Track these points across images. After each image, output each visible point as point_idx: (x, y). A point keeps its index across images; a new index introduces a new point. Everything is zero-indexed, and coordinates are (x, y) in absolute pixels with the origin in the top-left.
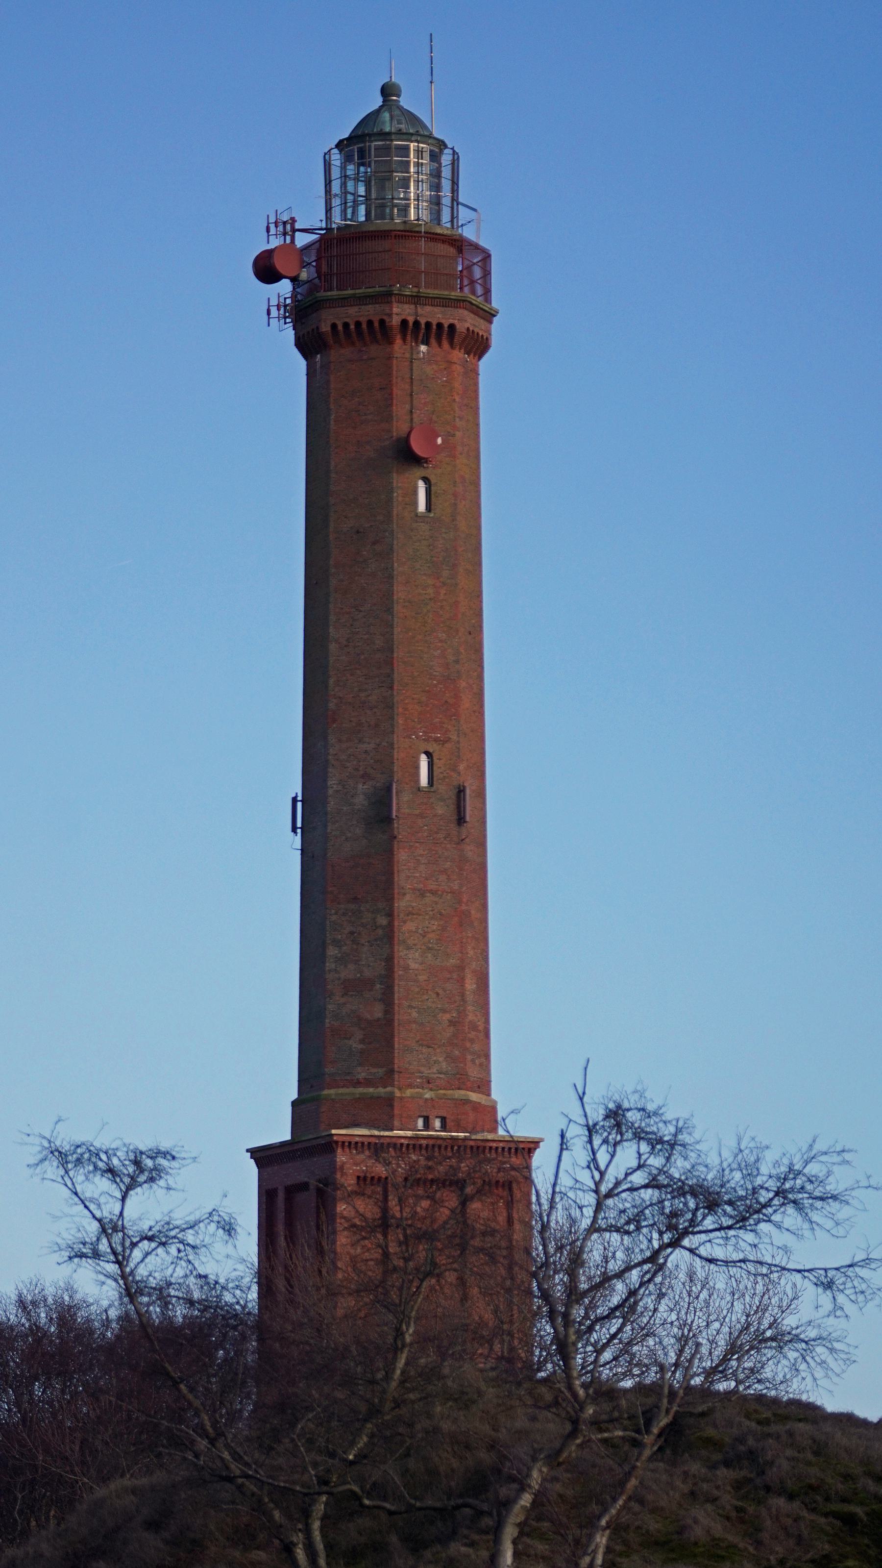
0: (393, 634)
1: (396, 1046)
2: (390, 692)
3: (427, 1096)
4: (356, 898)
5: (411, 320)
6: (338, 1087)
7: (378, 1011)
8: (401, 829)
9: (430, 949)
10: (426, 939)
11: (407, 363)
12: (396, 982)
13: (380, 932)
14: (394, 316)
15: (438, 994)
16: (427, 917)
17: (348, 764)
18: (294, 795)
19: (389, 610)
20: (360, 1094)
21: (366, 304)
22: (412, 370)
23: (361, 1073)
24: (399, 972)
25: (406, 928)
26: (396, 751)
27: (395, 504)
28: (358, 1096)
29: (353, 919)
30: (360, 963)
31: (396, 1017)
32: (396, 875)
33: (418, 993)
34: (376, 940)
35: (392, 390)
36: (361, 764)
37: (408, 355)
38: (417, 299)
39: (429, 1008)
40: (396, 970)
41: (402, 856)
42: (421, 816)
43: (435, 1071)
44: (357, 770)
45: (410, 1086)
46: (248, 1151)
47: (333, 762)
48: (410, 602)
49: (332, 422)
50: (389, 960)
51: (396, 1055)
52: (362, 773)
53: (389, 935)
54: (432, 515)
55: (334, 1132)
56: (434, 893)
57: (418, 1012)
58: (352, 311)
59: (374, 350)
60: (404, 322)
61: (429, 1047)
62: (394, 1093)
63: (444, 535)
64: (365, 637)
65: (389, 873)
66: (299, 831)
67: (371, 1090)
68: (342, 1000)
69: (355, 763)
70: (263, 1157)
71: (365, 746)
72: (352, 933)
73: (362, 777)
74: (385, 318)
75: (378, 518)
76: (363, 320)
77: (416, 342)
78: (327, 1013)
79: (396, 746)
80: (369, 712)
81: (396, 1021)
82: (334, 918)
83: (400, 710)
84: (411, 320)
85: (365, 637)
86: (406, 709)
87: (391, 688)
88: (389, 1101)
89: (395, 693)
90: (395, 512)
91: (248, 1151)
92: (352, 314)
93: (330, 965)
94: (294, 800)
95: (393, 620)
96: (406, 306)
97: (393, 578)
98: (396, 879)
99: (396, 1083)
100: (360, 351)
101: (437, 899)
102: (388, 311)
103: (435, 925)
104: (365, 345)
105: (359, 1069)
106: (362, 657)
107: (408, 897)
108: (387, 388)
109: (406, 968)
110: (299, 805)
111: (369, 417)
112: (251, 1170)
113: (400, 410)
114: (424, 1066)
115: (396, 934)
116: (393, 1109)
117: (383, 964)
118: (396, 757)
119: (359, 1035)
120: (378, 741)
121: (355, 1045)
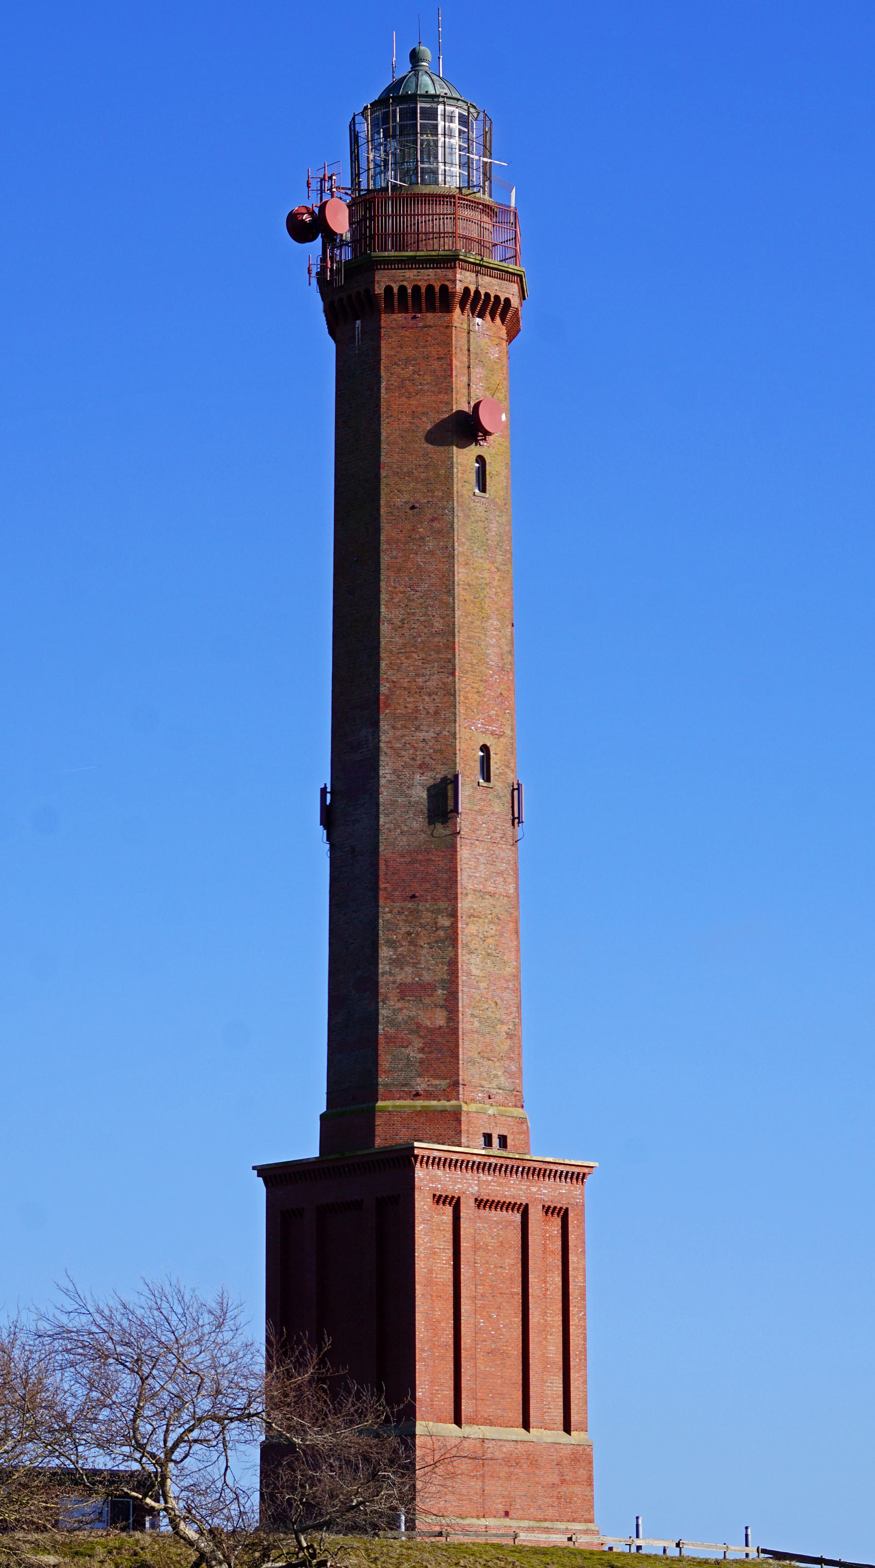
0: (454, 617)
1: (461, 1057)
2: (451, 678)
3: (490, 1112)
4: (413, 896)
5: (472, 288)
6: (394, 1099)
7: (440, 1019)
8: (464, 822)
9: (489, 955)
10: (486, 944)
11: (466, 334)
12: (460, 987)
13: (442, 933)
14: (458, 282)
15: (496, 1003)
16: (486, 921)
17: (403, 753)
18: (323, 786)
19: (450, 592)
20: (422, 1107)
21: (427, 268)
22: (469, 341)
23: (421, 1084)
24: (462, 978)
25: (467, 930)
26: (458, 741)
27: (455, 480)
28: (419, 1109)
30: (419, 966)
31: (460, 1026)
32: (459, 874)
33: (479, 1001)
34: (436, 942)
35: (451, 360)
36: (418, 753)
37: (465, 326)
38: (479, 268)
39: (489, 1018)
40: (460, 974)
41: (464, 853)
42: (480, 812)
43: (494, 1085)
44: (414, 759)
45: (473, 1100)
46: (254, 1168)
47: (385, 750)
48: (469, 585)
49: (383, 391)
50: (453, 965)
51: (461, 1066)
52: (419, 762)
53: (452, 937)
54: (487, 495)
55: (416, 1144)
56: (492, 895)
57: (480, 1022)
58: (411, 274)
59: (430, 317)
60: (467, 290)
61: (489, 1060)
62: (461, 1106)
63: (497, 518)
64: (422, 619)
65: (453, 871)
67: (434, 1103)
68: (399, 1005)
69: (411, 752)
70: (275, 1176)
71: (421, 735)
72: (409, 934)
73: (420, 767)
74: (447, 283)
75: (436, 494)
76: (423, 285)
77: (473, 314)
78: (380, 1018)
79: (458, 736)
80: (427, 698)
81: (460, 1030)
83: (462, 698)
84: (472, 288)
85: (422, 619)
86: (466, 698)
87: (453, 674)
88: (456, 1116)
89: (457, 680)
90: (455, 489)
91: (254, 1168)
92: (410, 277)
93: (383, 967)
94: (323, 791)
95: (454, 603)
96: (468, 274)
97: (453, 557)
98: (459, 878)
99: (461, 1096)
100: (414, 318)
101: (494, 903)
102: (451, 277)
103: (493, 930)
104: (420, 312)
105: (419, 1080)
106: (419, 640)
107: (470, 897)
108: (446, 359)
109: (469, 974)
110: (329, 796)
111: (426, 388)
112: (259, 1187)
113: (459, 381)
114: (485, 1080)
115: (460, 937)
116: (460, 1124)
117: (446, 968)
118: (458, 748)
119: (418, 1043)
120: (438, 729)
121: (413, 1053)
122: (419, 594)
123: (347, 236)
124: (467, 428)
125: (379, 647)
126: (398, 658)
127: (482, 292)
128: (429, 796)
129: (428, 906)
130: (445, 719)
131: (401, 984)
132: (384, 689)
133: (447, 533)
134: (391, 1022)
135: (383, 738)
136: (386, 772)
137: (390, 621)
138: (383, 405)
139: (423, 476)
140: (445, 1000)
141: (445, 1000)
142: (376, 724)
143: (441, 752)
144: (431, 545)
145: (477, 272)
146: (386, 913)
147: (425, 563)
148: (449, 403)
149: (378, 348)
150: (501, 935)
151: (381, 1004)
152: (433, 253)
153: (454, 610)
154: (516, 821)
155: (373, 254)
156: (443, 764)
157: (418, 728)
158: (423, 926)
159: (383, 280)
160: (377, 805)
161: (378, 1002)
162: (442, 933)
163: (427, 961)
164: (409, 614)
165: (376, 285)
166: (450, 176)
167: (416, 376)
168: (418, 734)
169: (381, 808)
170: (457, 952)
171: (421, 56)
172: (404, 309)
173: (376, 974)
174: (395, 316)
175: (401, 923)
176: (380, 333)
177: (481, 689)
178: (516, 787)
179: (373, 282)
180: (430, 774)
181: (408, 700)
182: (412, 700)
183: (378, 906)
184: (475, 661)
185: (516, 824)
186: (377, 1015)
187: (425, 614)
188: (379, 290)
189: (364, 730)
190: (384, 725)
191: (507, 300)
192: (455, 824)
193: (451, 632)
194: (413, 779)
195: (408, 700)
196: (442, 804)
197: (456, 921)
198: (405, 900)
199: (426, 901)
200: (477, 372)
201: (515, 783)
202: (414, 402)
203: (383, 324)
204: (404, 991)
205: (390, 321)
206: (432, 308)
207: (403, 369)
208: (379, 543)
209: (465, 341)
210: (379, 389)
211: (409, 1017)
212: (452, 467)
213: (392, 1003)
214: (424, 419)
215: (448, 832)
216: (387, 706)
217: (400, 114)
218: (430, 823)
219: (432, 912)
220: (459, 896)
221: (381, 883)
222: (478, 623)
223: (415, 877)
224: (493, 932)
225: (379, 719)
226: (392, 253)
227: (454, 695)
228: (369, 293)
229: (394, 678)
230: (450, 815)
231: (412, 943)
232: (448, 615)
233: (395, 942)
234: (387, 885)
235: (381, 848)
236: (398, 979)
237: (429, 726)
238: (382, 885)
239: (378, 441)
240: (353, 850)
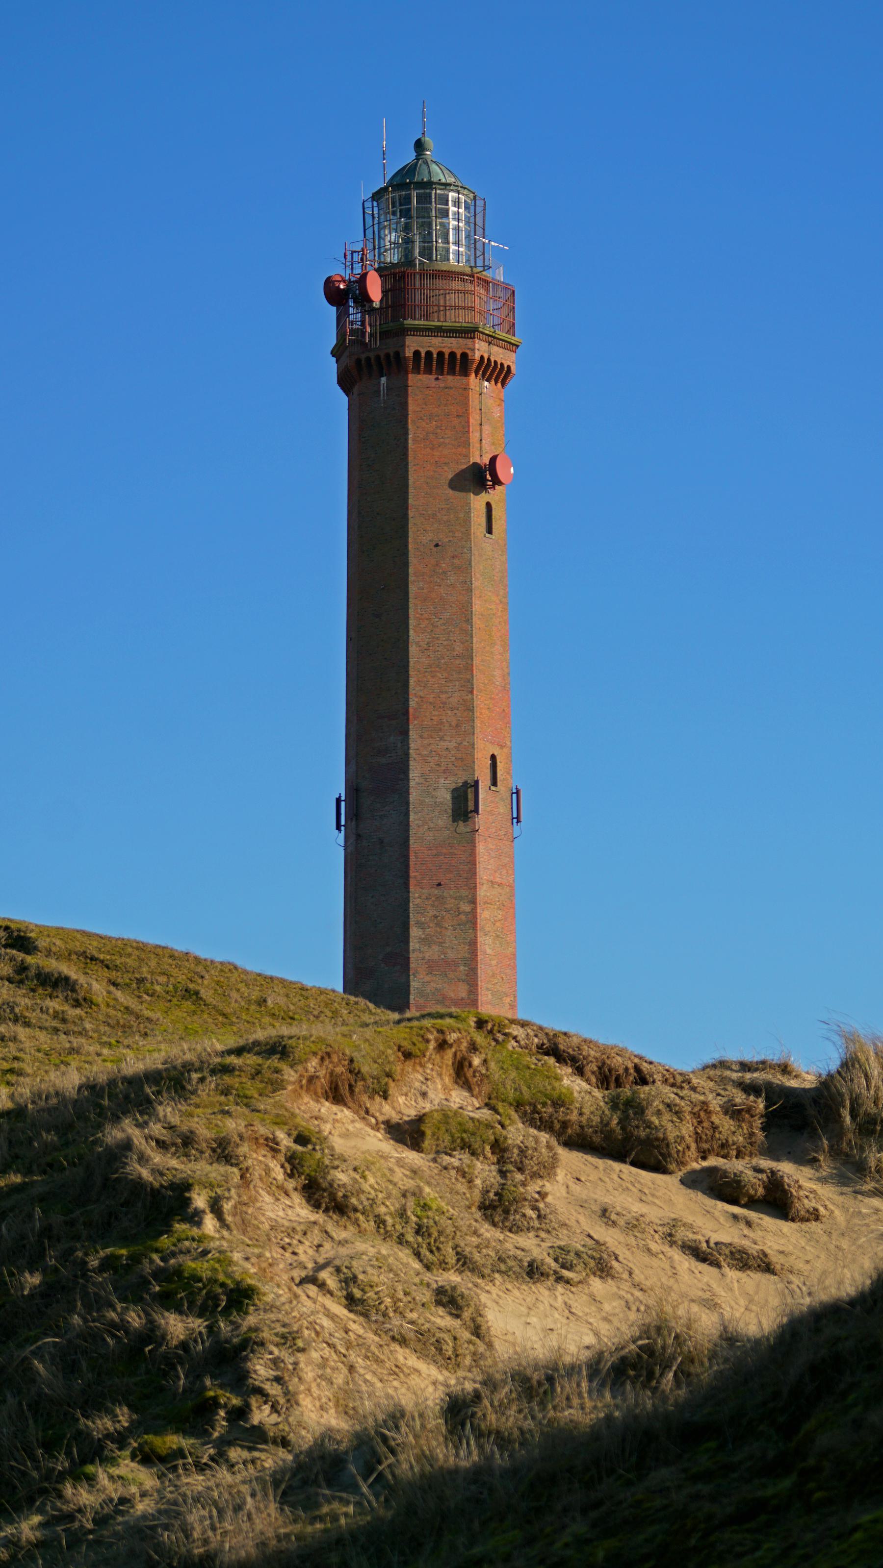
2: (470, 696)
5: (486, 356)
7: (462, 991)
8: (481, 820)
9: (498, 936)
11: (478, 396)
13: (463, 917)
14: (476, 351)
17: (430, 759)
19: (469, 621)
22: (480, 402)
24: (480, 957)
25: (484, 915)
29: (436, 903)
35: (469, 418)
37: (478, 389)
38: (492, 339)
41: (481, 848)
49: (410, 442)
50: (473, 944)
57: (492, 995)
60: (482, 357)
64: (445, 643)
65: (473, 863)
66: (343, 828)
68: (427, 978)
69: (437, 758)
72: (436, 917)
73: (444, 772)
74: (467, 351)
75: (456, 534)
76: (447, 352)
78: (412, 989)
80: (449, 712)
82: (418, 900)
85: (445, 643)
86: (481, 714)
87: (472, 692)
93: (413, 944)
94: (338, 801)
100: (437, 379)
102: (471, 346)
104: (442, 374)
108: (464, 415)
109: (485, 953)
110: (343, 804)
122: (442, 621)
123: (376, 304)
124: (481, 477)
125: (408, 666)
126: (425, 676)
127: (493, 360)
128: (454, 798)
129: (451, 893)
130: (465, 731)
131: (429, 960)
132: (413, 703)
133: (465, 569)
134: (421, 994)
135: (412, 745)
136: (415, 775)
137: (417, 644)
138: (410, 453)
139: (445, 518)
140: (467, 975)
141: (467, 975)
142: (405, 733)
143: (462, 759)
144: (452, 579)
145: (490, 343)
146: (416, 896)
147: (447, 594)
148: (467, 456)
149: (406, 403)
150: (506, 919)
151: (412, 977)
152: (457, 324)
153: (472, 637)
154: (515, 821)
155: (406, 322)
156: (464, 770)
157: (442, 739)
158: (447, 911)
159: (413, 345)
160: (407, 803)
161: (409, 976)
162: (463, 917)
163: (451, 941)
164: (434, 638)
165: (407, 349)
166: (456, 255)
167: (439, 431)
168: (442, 743)
169: (411, 807)
170: (476, 934)
171: (426, 146)
172: (428, 371)
173: (407, 951)
174: (420, 377)
175: (429, 908)
176: (407, 391)
177: (491, 706)
178: (515, 791)
179: (403, 345)
180: (452, 779)
181: (434, 713)
182: (437, 713)
183: (409, 892)
184: (486, 682)
185: (515, 824)
186: (409, 986)
187: (448, 639)
188: (409, 354)
189: (392, 738)
190: (413, 734)
191: (509, 367)
192: (474, 823)
193: (469, 655)
194: (438, 782)
195: (434, 713)
196: (464, 804)
197: (476, 907)
198: (432, 888)
199: (450, 889)
200: (486, 429)
201: (514, 788)
202: (437, 453)
203: (410, 383)
204: (431, 966)
205: (417, 382)
206: (452, 371)
207: (427, 424)
208: (408, 575)
209: (477, 402)
210: (406, 440)
211: (436, 989)
212: (470, 512)
213: (422, 977)
214: (446, 468)
215: (469, 830)
216: (415, 718)
217: (408, 195)
218: (454, 821)
219: (455, 898)
220: (478, 885)
221: (411, 872)
222: (488, 648)
223: (440, 868)
224: (500, 917)
225: (408, 729)
226: (422, 322)
227: (473, 711)
228: (399, 357)
229: (421, 694)
230: (470, 815)
231: (438, 925)
232: (467, 641)
233: (423, 923)
234: (416, 874)
235: (411, 842)
236: (427, 955)
237: (452, 737)
238: (412, 874)
239: (406, 486)
240: (381, 841)
